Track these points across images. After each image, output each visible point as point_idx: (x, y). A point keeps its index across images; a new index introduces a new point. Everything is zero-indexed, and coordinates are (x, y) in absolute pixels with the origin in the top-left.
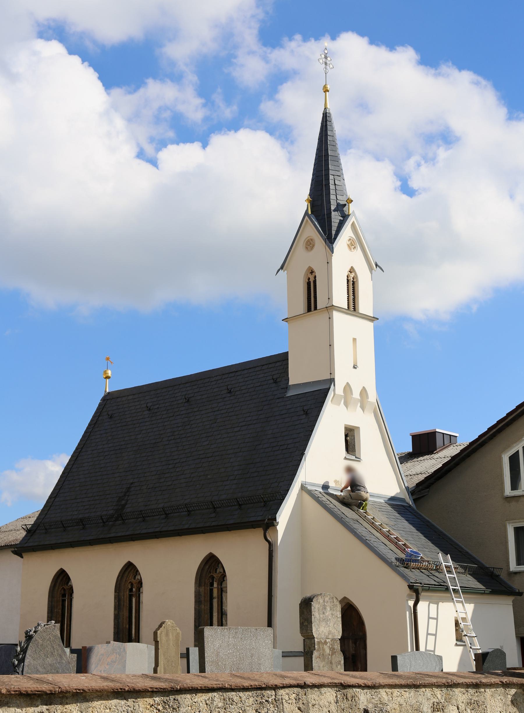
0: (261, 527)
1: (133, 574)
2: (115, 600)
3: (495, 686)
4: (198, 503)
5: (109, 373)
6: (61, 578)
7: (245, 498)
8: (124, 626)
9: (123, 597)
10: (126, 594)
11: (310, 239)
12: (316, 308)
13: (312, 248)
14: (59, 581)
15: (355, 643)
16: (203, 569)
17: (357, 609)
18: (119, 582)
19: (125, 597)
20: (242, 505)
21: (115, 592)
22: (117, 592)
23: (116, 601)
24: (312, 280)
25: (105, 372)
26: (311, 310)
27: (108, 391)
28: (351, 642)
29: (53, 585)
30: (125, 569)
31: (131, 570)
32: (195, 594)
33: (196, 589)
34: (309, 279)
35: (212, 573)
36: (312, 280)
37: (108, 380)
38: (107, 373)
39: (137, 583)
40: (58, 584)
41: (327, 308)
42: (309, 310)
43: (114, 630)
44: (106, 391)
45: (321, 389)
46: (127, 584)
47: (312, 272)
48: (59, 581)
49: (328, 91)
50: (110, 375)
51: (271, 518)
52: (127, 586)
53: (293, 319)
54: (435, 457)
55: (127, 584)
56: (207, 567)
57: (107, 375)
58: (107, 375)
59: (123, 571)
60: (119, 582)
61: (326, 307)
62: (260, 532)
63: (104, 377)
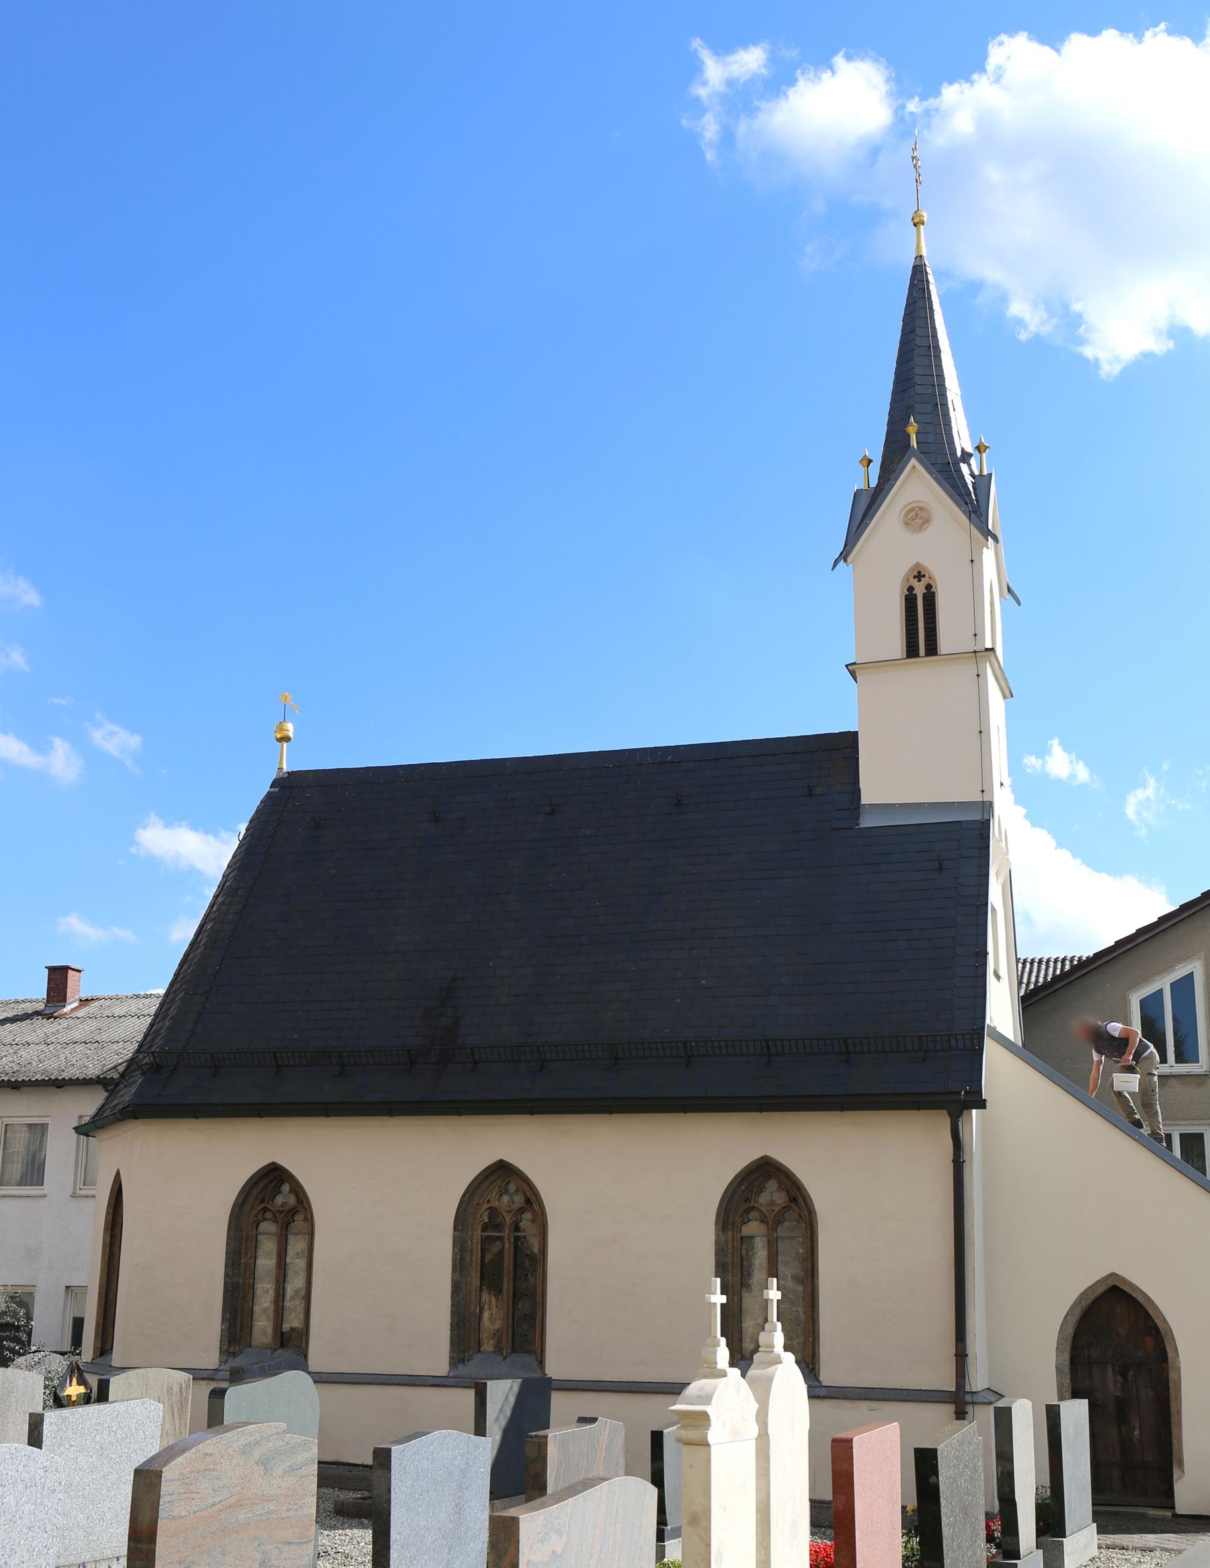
0: (943, 1109)
1: (499, 1190)
2: (453, 1248)
3: (455, 1355)
4: (719, 1041)
5: (290, 728)
6: (262, 1185)
7: (805, 1041)
8: (472, 1308)
9: (469, 1242)
10: (477, 1235)
11: (918, 507)
12: (932, 650)
13: (921, 528)
14: (254, 1193)
15: (1124, 1375)
16: (733, 1194)
17: (1145, 1303)
18: (463, 1206)
19: (474, 1241)
20: (850, 1053)
21: (455, 1228)
22: (459, 1230)
23: (456, 1250)
24: (920, 590)
25: (281, 728)
26: (919, 654)
27: (285, 768)
28: (1110, 1370)
29: (241, 1200)
30: (482, 1177)
31: (495, 1180)
32: (716, 1249)
33: (717, 1235)
34: (911, 589)
35: (752, 1202)
36: (920, 590)
37: (285, 744)
38: (284, 728)
39: (513, 1212)
40: (251, 1199)
41: (977, 654)
42: (912, 651)
43: (452, 1319)
44: (280, 769)
45: (960, 821)
46: (481, 1212)
47: (919, 576)
48: (254, 1193)
49: (923, 224)
50: (291, 734)
51: (169, 1049)
52: (481, 1216)
53: (872, 667)
54: (1033, 979)
55: (481, 1212)
56: (743, 1187)
57: (285, 733)
58: (286, 735)
59: (479, 1181)
60: (463, 1206)
61: (975, 652)
62: (941, 1122)
63: (279, 736)
